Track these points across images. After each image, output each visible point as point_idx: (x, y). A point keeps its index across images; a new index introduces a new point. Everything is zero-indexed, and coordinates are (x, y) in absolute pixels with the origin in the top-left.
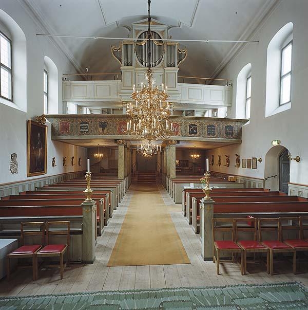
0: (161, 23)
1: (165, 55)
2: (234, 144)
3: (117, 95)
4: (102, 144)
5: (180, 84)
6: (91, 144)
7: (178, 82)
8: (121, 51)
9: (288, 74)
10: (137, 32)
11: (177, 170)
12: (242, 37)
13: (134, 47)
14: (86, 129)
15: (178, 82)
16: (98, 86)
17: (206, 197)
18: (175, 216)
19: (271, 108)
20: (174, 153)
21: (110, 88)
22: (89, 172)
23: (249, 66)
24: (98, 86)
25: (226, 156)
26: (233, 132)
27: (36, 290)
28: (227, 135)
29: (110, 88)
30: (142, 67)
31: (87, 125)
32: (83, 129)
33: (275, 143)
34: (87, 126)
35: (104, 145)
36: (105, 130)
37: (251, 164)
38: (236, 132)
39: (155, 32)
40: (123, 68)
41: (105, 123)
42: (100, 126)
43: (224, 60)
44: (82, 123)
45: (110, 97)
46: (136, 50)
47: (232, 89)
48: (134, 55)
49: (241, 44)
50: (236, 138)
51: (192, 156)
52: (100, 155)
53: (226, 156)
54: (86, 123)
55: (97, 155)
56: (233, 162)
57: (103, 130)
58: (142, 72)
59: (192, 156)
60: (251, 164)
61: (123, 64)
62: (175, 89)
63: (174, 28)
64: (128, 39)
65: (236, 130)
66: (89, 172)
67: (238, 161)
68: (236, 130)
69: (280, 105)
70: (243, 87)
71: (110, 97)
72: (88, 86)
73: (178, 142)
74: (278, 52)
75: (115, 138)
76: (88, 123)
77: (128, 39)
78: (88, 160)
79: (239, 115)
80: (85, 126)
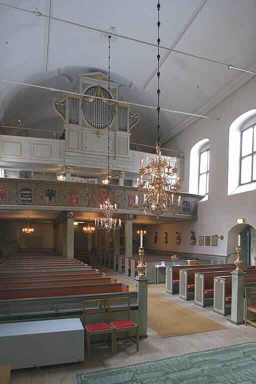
0: (115, 81)
1: (116, 117)
2: (189, 220)
3: (60, 157)
4: (32, 215)
5: (131, 151)
6: (20, 216)
7: (130, 149)
8: (65, 106)
9: (249, 155)
10: (84, 85)
11: (113, 249)
12: (200, 111)
13: (81, 103)
14: (28, 197)
15: (130, 149)
16: (37, 144)
17: (237, 268)
18: (163, 295)
19: (233, 189)
20: (131, 228)
21: (51, 148)
22: (141, 247)
23: (206, 140)
24: (37, 144)
25: (177, 233)
26: (191, 209)
27: (126, 360)
28: (184, 211)
29: (51, 148)
30: (91, 128)
31: (30, 192)
32: (25, 197)
33: (240, 221)
34: (31, 194)
35: (39, 217)
36: (53, 200)
37: (211, 241)
38: (193, 208)
39: (104, 89)
40: (67, 126)
41: (52, 191)
42: (47, 195)
43: (173, 131)
44: (25, 190)
45: (51, 159)
46: (82, 106)
47: (184, 161)
48: (81, 112)
49: (197, 118)
50: (193, 215)
51: (24, 230)
52: (30, 230)
53: (177, 233)
54: (28, 190)
55: (26, 230)
56: (187, 239)
57: (50, 199)
58: (89, 132)
59: (24, 230)
60: (211, 241)
61: (67, 120)
62: (127, 156)
63: (123, 87)
64: (78, 94)
65: (192, 205)
66: (141, 247)
67: (193, 238)
68: (192, 205)
69: (240, 185)
70: (199, 161)
71: (51, 159)
72: (22, 143)
73: (135, 216)
74: (239, 134)
75: (64, 210)
76: (31, 191)
77: (78, 94)
78: (239, 236)
79: (193, 190)
80: (26, 194)
